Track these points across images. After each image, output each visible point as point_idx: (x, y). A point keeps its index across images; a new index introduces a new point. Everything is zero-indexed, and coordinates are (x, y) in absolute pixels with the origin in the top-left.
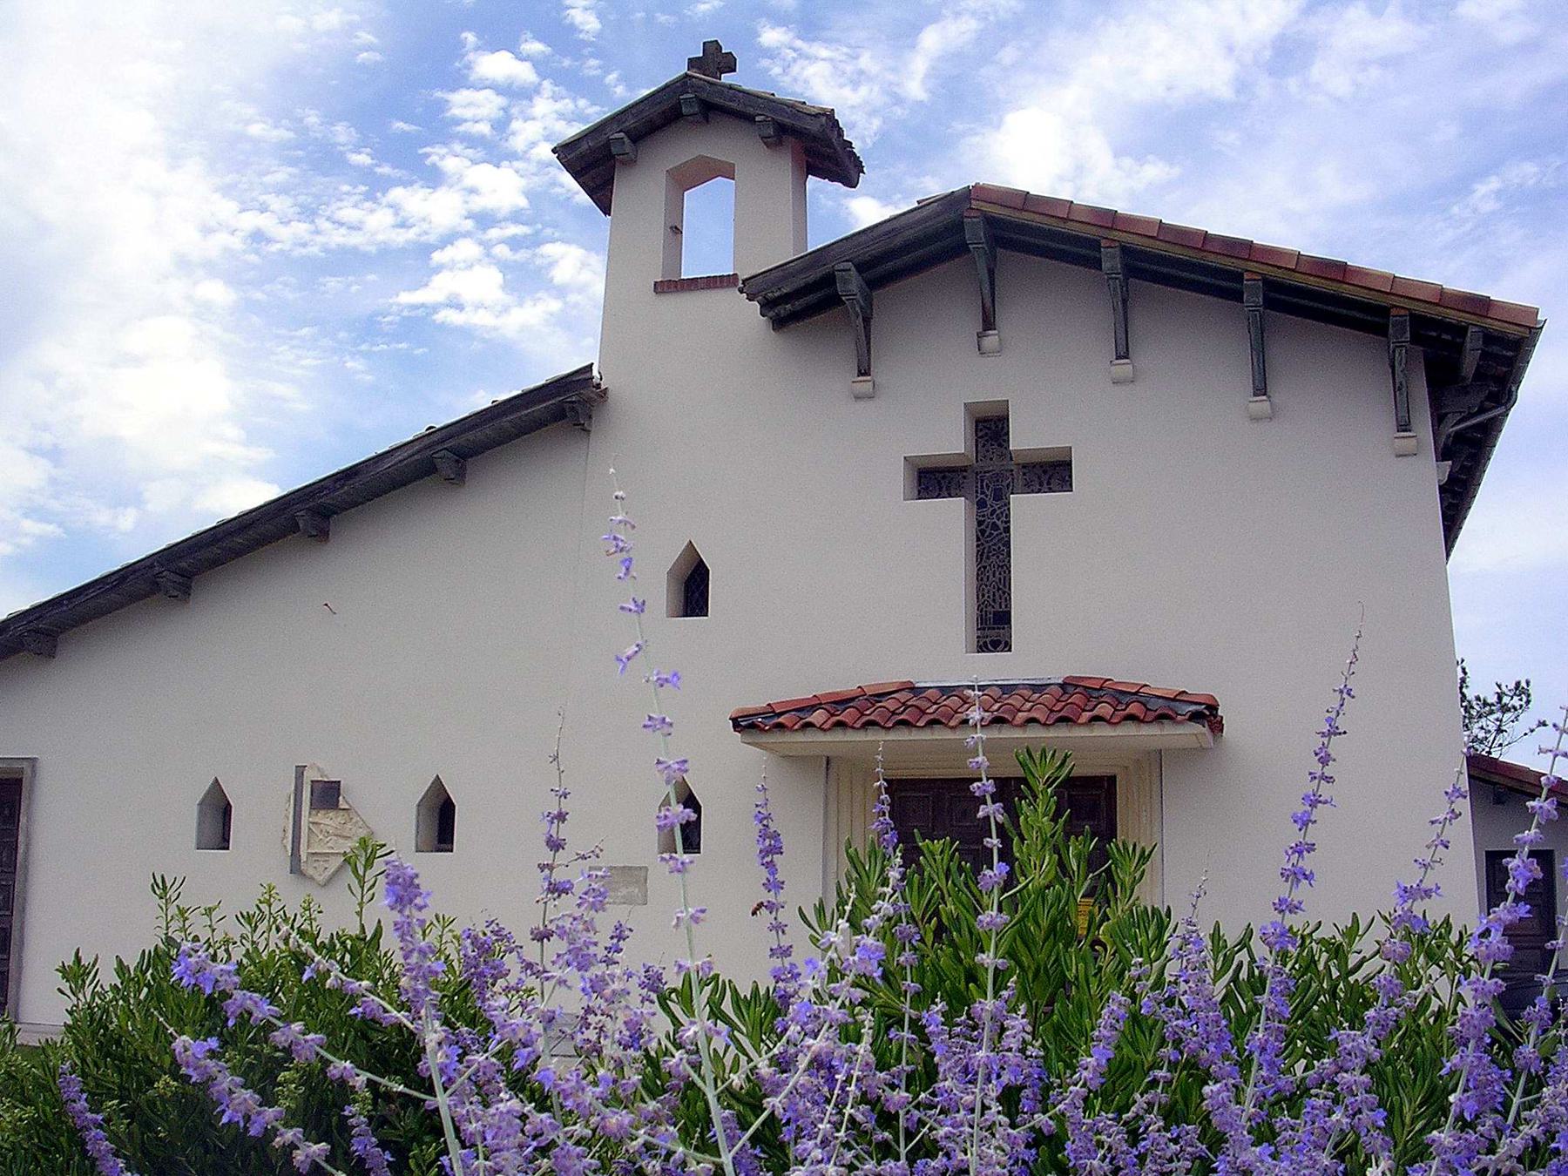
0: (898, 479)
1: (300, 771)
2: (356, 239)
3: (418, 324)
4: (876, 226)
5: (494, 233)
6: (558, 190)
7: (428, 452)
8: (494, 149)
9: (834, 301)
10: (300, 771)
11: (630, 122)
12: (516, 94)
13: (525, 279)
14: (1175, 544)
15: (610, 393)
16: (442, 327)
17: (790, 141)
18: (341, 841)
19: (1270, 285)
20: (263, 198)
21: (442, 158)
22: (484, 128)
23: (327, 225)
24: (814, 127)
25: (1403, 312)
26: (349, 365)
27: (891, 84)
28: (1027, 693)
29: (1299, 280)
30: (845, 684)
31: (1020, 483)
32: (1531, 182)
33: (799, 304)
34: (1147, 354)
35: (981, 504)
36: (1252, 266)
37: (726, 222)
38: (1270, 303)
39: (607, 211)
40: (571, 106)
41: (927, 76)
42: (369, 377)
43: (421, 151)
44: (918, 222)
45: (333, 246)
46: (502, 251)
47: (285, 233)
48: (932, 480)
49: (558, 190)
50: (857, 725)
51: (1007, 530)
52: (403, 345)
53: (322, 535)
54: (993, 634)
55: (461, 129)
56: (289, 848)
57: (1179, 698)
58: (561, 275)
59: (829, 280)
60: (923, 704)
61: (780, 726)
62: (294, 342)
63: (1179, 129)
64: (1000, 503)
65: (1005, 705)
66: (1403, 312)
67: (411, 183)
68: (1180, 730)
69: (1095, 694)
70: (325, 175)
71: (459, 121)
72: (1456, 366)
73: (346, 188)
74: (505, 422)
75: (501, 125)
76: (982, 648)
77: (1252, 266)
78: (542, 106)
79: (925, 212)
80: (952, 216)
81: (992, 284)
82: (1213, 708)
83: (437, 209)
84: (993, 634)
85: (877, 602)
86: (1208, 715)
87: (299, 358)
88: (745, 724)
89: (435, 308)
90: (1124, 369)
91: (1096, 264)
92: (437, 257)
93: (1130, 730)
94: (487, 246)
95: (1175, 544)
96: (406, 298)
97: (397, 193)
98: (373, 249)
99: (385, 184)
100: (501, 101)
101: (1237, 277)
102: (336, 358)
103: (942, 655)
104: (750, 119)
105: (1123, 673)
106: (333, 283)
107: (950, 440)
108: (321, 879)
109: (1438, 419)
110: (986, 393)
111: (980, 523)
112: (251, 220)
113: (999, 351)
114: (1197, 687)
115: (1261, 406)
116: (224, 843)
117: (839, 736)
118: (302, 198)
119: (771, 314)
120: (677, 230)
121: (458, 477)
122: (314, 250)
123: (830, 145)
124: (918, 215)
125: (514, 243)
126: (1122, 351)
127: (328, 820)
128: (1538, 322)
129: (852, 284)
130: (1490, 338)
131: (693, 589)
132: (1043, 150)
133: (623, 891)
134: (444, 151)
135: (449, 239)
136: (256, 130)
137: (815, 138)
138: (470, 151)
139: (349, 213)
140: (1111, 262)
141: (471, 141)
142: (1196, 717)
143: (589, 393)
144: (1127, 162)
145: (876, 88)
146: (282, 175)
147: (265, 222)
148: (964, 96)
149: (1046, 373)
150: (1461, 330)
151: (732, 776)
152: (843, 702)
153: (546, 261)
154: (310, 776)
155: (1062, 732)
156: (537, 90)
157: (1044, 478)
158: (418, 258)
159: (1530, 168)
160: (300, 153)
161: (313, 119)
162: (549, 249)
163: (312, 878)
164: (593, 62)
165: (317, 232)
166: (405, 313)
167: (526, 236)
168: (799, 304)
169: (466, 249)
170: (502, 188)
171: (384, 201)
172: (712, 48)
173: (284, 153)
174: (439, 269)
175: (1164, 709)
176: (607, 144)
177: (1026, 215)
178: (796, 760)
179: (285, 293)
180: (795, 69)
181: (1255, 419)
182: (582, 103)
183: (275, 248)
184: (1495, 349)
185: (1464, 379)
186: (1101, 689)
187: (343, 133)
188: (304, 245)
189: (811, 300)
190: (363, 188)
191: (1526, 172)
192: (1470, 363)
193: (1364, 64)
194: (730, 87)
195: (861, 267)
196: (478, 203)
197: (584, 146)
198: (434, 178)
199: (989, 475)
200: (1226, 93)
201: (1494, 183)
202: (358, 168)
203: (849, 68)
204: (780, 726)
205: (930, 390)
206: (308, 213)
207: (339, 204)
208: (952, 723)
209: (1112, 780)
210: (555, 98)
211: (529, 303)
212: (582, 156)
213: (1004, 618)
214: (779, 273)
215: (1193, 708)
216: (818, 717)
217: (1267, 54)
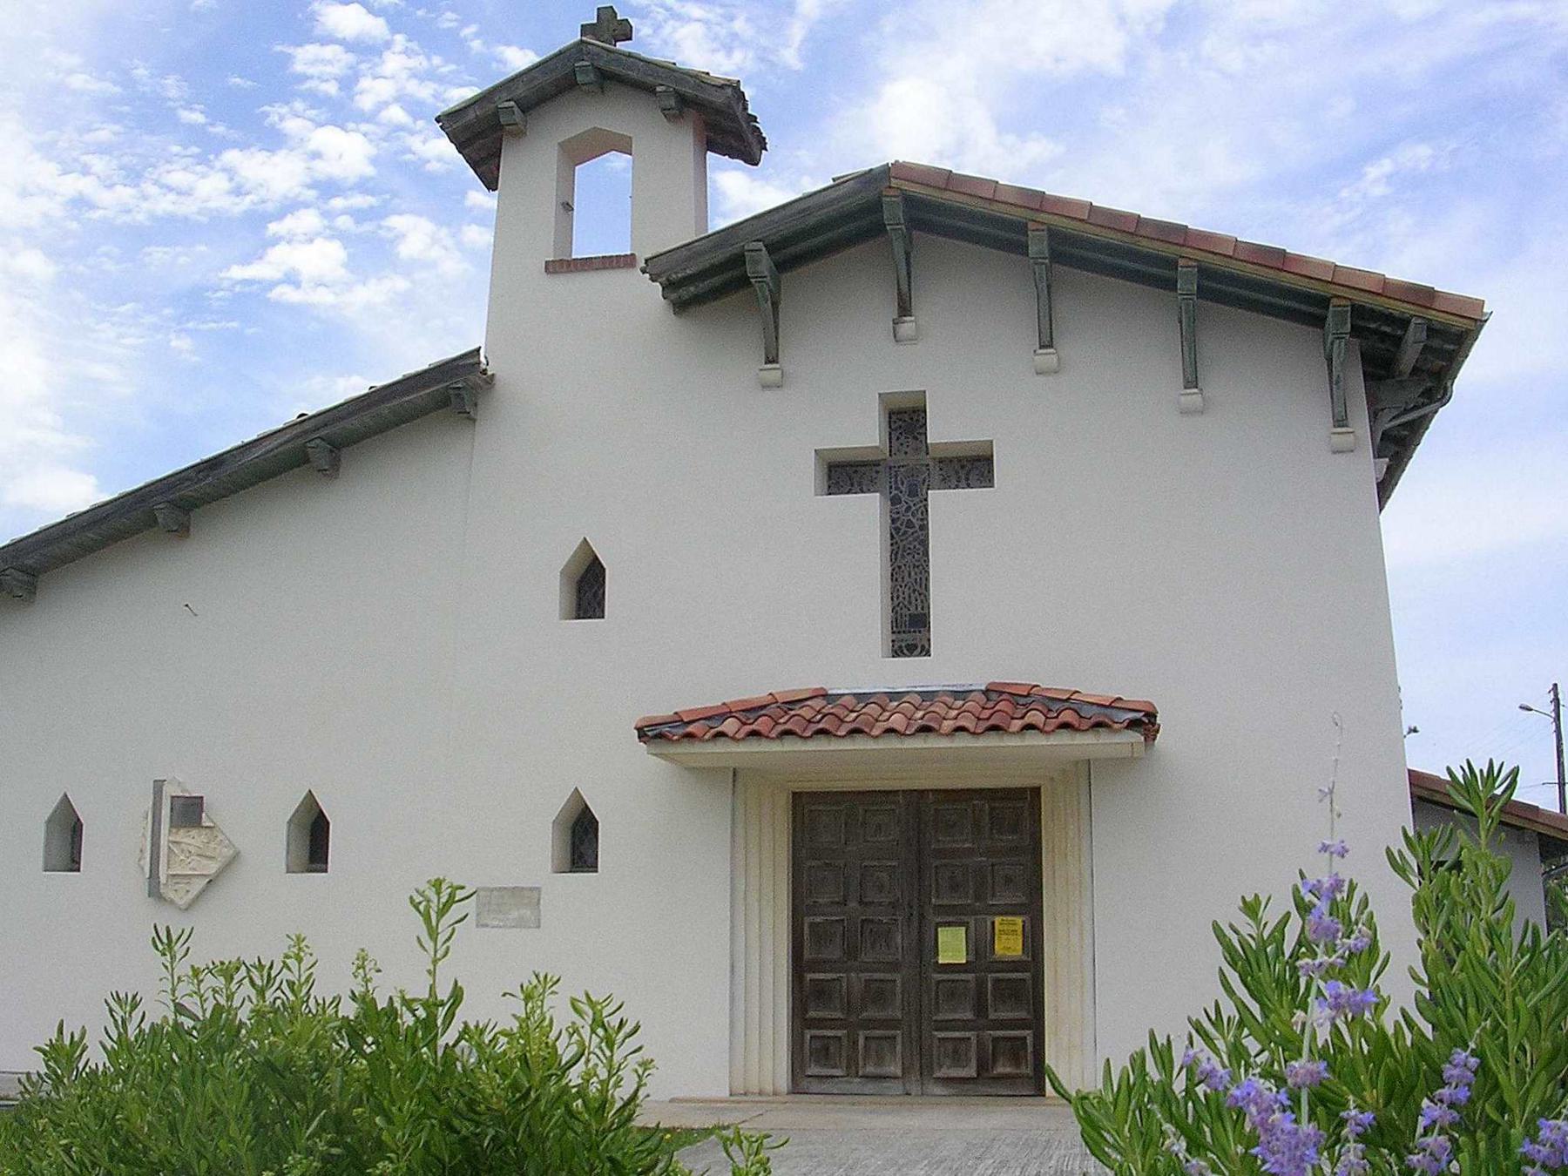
0: (808, 473)
1: (158, 786)
2: (188, 208)
3: (252, 300)
4: (784, 207)
5: (338, 203)
6: (408, 157)
7: (300, 441)
8: (339, 112)
9: (744, 282)
10: (158, 786)
11: (521, 91)
12: (366, 50)
13: (370, 252)
14: (1095, 544)
15: (496, 381)
16: (278, 306)
17: (692, 113)
18: (205, 862)
19: (1204, 272)
20: (85, 158)
21: (282, 119)
22: (331, 88)
23: (153, 190)
24: (718, 99)
25: (1343, 302)
26: (173, 344)
27: (765, 49)
28: (949, 700)
29: (1237, 268)
30: (754, 690)
31: (936, 477)
32: (1423, 166)
33: (703, 286)
34: (1071, 347)
35: (895, 501)
36: (1186, 251)
37: (620, 197)
38: (1203, 293)
39: (491, 184)
40: (425, 63)
41: (805, 41)
42: (195, 359)
43: (258, 111)
44: (832, 202)
45: (159, 212)
46: (344, 222)
47: (106, 197)
48: (843, 474)
49: (408, 157)
50: (773, 735)
51: (924, 528)
52: (235, 324)
53: (181, 531)
54: (909, 638)
55: (308, 85)
56: (147, 869)
57: (1115, 705)
58: (408, 249)
59: (738, 260)
60: (841, 712)
61: (690, 736)
62: (115, 319)
63: (1063, 102)
64: (916, 499)
65: (927, 714)
66: (1343, 302)
67: (249, 147)
68: (1117, 739)
69: (1022, 701)
70: (152, 132)
71: (306, 78)
72: (1393, 358)
73: (176, 149)
74: (385, 409)
75: (348, 82)
76: (897, 652)
77: (1186, 251)
78: (393, 63)
79: (842, 190)
80: (869, 195)
81: (908, 264)
82: (1151, 715)
83: (275, 173)
84: (909, 638)
85: (793, 608)
86: (1145, 723)
87: (120, 336)
88: (651, 733)
89: (273, 284)
90: (1048, 358)
91: (1022, 249)
92: (273, 228)
93: (1064, 739)
94: (327, 215)
95: (1095, 544)
96: (238, 272)
97: (231, 156)
98: (205, 220)
99: (222, 145)
100: (351, 58)
101: (1172, 264)
102: (160, 336)
103: (859, 663)
104: (650, 90)
105: (1054, 680)
106: (158, 255)
107: (864, 433)
108: (182, 901)
109: (1374, 416)
110: (903, 383)
111: (893, 521)
112: (74, 184)
113: (913, 340)
114: (1134, 693)
115: (1193, 398)
116: (74, 864)
117: (755, 747)
118: (126, 159)
119: (674, 296)
120: (568, 207)
121: (331, 470)
122: (141, 217)
123: (735, 119)
124: (833, 194)
125: (359, 215)
126: (1046, 340)
127: (192, 839)
128: (1483, 314)
129: (762, 265)
130: (1432, 331)
131: (587, 589)
132: (918, 118)
133: (515, 914)
134: (284, 110)
135: (290, 207)
136: (78, 81)
137: (718, 111)
138: (314, 112)
139: (178, 178)
140: (1038, 246)
141: (315, 100)
142: (1133, 724)
143: (474, 378)
144: (1010, 139)
145: (751, 55)
146: (105, 134)
147: (86, 185)
148: (841, 60)
149: (969, 365)
150: (1404, 323)
151: (633, 793)
152: (753, 710)
153: (391, 235)
154: (170, 790)
155: (992, 741)
156: (388, 45)
157: (962, 474)
158: (254, 227)
159: (1424, 151)
160: (126, 109)
161: (141, 72)
162: (395, 221)
163: (172, 902)
164: (449, 15)
165: (145, 198)
166: (238, 289)
167: (372, 207)
168: (703, 286)
169: (308, 220)
170: (347, 151)
171: (218, 164)
172: (606, 14)
173: (106, 108)
174: (276, 240)
175: (1101, 717)
176: (496, 113)
177: (947, 195)
178: (703, 773)
179: (101, 264)
180: (667, 30)
181: (1185, 412)
182: (436, 60)
183: (97, 214)
184: (1436, 343)
185: (1401, 373)
186: (1028, 695)
187: (172, 86)
188: (129, 211)
189: (722, 282)
190: (195, 150)
191: (1419, 154)
192: (1409, 356)
193: (1256, 39)
194: (630, 55)
195: (772, 248)
196: (323, 169)
197: (471, 115)
198: (273, 140)
199: (905, 468)
200: (1115, 67)
201: (1386, 165)
202: (192, 128)
203: (723, 32)
204: (690, 736)
205: (841, 378)
206: (134, 176)
207: (168, 167)
208: (875, 732)
209: (1036, 791)
210: (407, 52)
211: (373, 281)
212: (466, 127)
213: (920, 621)
214: (685, 252)
215: (1131, 715)
216: (730, 726)
217: (1160, 26)
